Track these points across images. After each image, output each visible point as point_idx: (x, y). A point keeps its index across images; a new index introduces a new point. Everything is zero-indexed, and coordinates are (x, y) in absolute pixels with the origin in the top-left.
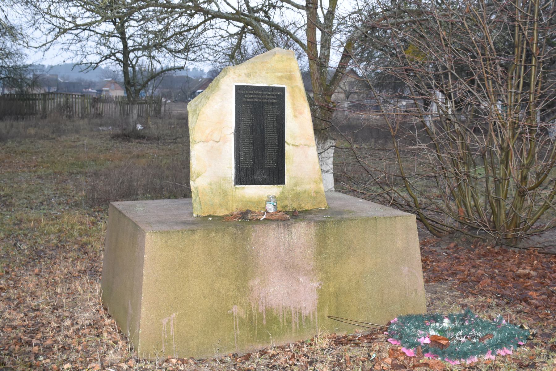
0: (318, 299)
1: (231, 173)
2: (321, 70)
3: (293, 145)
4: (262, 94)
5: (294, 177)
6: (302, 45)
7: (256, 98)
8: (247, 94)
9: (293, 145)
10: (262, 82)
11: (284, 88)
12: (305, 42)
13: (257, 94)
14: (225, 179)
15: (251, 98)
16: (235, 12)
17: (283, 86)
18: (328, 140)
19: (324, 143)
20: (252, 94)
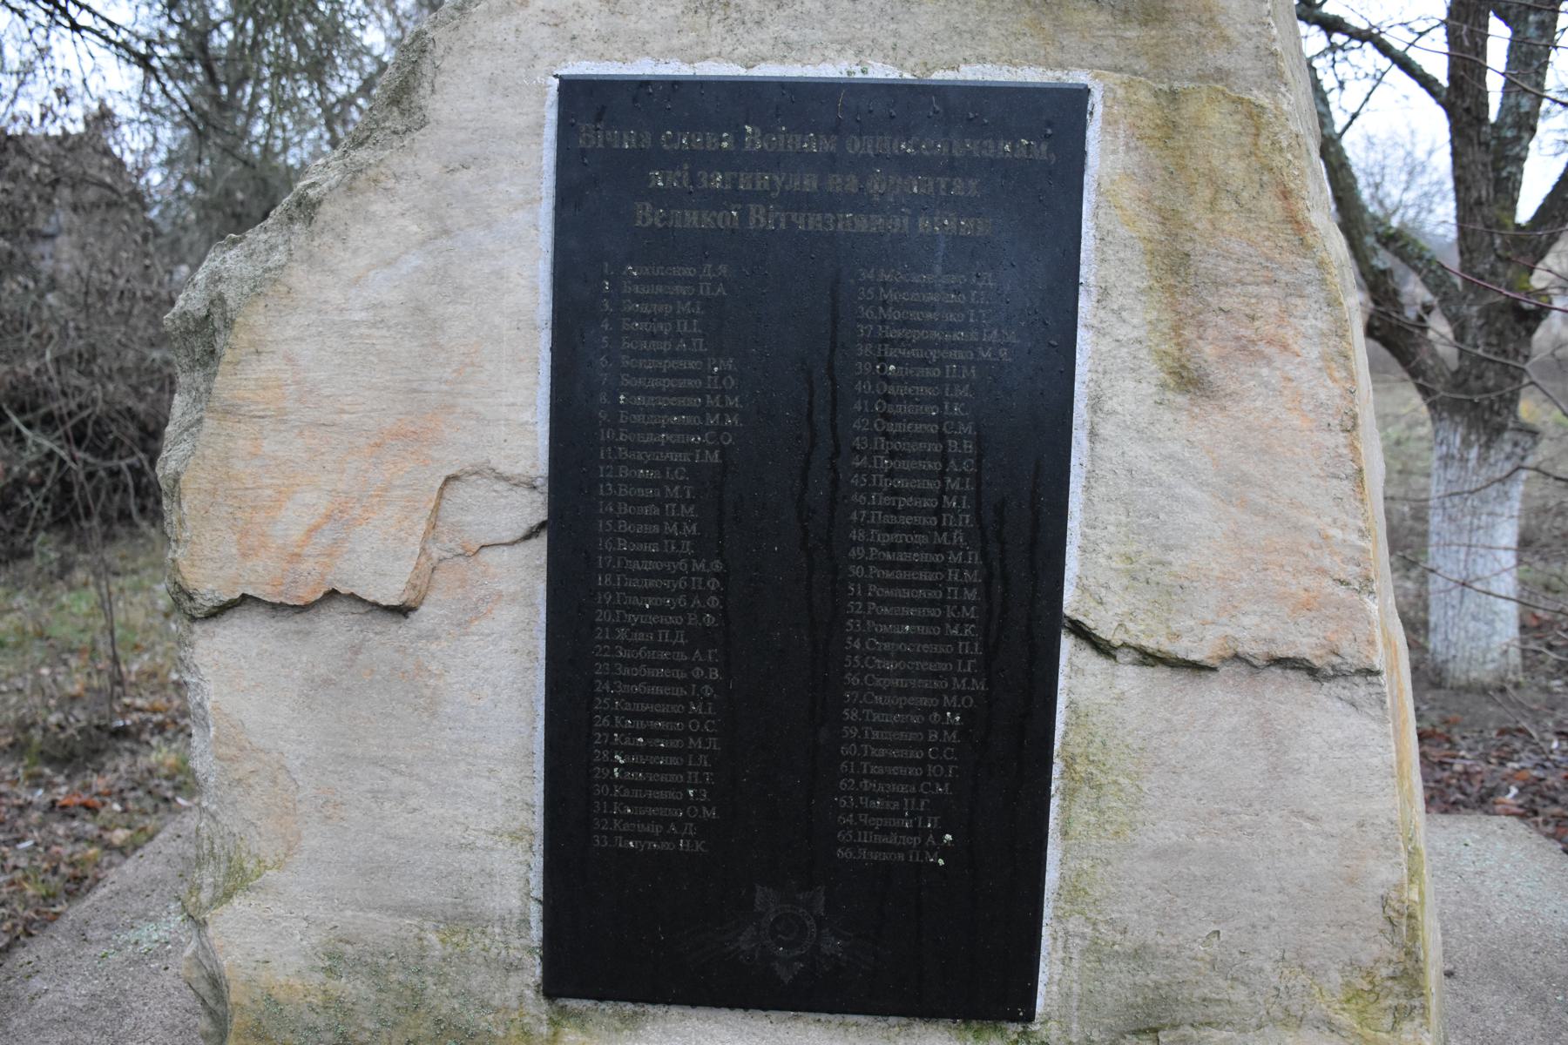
0: (1470, 427)
1: (513, 881)
2: (1497, 170)
3: (1148, 658)
4: (831, 163)
5: (1139, 954)
6: (1426, 82)
7: (762, 197)
8: (670, 161)
9: (1148, 658)
10: (844, 44)
11: (1080, 95)
12: (1438, 68)
13: (772, 161)
14: (462, 920)
15: (717, 200)
16: (1338, 129)
17: (1079, 77)
18: (1507, 435)
19: (1487, 446)
20: (722, 161)
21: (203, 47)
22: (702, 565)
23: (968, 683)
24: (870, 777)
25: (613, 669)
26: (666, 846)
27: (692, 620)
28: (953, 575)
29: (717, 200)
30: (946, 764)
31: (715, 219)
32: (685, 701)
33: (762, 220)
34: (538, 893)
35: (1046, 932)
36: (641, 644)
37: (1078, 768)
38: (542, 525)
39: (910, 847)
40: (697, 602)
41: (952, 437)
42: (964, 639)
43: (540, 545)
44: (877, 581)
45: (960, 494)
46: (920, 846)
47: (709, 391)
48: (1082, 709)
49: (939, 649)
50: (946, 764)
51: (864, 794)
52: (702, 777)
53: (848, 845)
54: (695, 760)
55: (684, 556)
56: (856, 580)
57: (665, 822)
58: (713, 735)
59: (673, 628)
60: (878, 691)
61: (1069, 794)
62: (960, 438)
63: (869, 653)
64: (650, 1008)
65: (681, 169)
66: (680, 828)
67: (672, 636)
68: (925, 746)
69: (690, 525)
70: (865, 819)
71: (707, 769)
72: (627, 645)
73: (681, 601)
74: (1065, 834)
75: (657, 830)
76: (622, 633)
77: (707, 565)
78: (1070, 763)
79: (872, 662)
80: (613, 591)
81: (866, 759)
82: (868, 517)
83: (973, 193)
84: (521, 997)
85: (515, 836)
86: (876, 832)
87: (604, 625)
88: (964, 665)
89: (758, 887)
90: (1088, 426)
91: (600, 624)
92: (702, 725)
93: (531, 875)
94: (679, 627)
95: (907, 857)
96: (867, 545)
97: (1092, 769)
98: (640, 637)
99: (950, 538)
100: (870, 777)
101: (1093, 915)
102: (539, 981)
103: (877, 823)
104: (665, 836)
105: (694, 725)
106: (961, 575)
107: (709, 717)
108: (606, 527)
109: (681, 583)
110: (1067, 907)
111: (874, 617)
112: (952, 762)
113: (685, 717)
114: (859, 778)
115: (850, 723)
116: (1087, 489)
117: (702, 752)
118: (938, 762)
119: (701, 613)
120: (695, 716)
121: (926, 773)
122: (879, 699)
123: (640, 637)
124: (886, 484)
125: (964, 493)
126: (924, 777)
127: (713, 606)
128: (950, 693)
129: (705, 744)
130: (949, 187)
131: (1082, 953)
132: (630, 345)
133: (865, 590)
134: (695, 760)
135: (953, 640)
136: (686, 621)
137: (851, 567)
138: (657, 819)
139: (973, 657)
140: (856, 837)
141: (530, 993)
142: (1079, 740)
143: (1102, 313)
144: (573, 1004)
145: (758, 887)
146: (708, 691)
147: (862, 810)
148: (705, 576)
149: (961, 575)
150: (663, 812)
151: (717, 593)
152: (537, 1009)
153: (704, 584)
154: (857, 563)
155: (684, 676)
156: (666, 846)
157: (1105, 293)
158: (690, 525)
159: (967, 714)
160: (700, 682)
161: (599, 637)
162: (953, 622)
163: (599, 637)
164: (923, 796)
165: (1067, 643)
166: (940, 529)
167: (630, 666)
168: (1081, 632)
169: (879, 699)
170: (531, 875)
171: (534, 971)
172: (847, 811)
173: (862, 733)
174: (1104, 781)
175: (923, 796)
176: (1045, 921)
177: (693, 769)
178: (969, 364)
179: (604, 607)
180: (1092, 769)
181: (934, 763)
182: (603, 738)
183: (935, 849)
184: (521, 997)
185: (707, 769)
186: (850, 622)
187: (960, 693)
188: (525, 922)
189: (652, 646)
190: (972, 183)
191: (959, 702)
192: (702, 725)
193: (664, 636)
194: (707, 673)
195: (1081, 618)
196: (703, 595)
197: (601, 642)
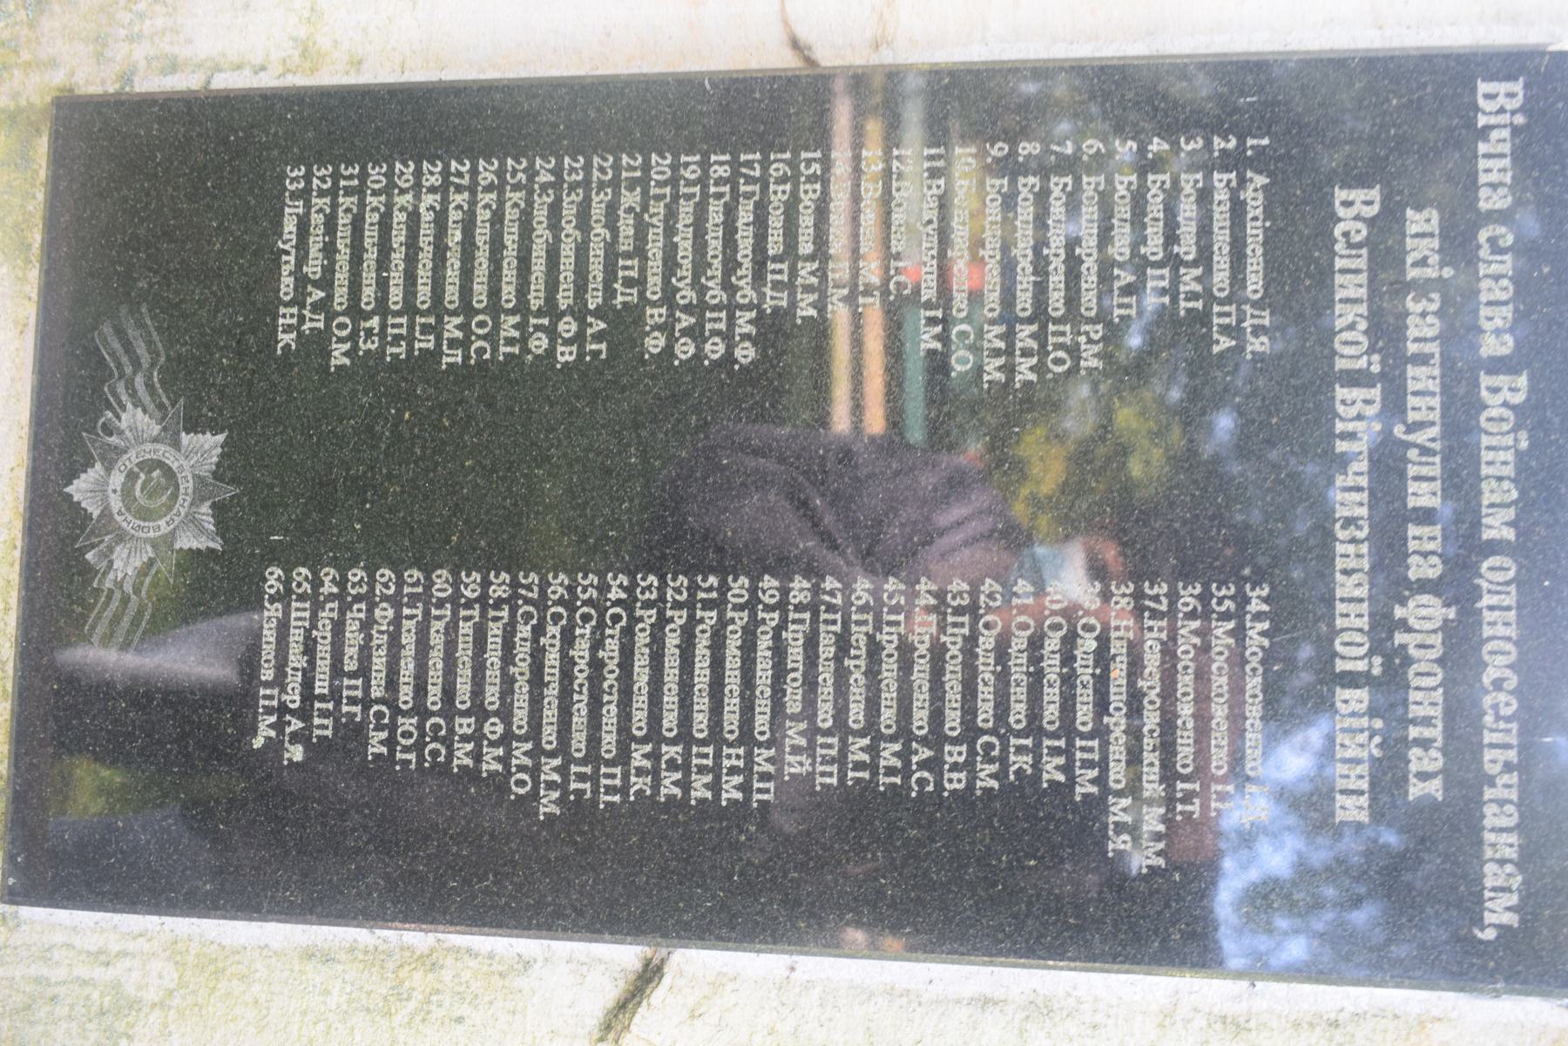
21: (1193, 394)
22: (749, 329)
23: (551, 785)
24: (397, 621)
25: (573, 187)
26: (287, 283)
27: (656, 315)
28: (733, 757)
29: (1386, 330)
30: (419, 747)
31: (1352, 327)
32: (522, 307)
33: (1353, 411)
34: (221, 82)
35: (150, 922)
36: (615, 231)
37: (418, 975)
38: (810, 62)
39: (283, 690)
40: (686, 321)
41: (972, 752)
42: (626, 776)
43: (782, 60)
44: (723, 623)
45: (873, 767)
46: (283, 709)
47: (1043, 328)
48: (520, 982)
49: (609, 740)
50: (419, 747)
51: (370, 611)
52: (397, 339)
53: (878, 599)
54: (426, 329)
55: (762, 296)
56: (724, 588)
57: (326, 282)
58: (466, 357)
59: (641, 282)
60: (539, 631)
61: (374, 959)
62: (969, 766)
63: (601, 616)
64: (34, 274)
65: (1442, 264)
66: (316, 308)
67: (628, 282)
68: (449, 710)
69: (814, 305)
70: (328, 614)
71: (410, 348)
72: (612, 208)
73: (687, 295)
74: (308, 954)
75: (313, 269)
76: (630, 199)
77: (745, 337)
78: (429, 962)
79: (586, 618)
80: (703, 181)
81: (427, 613)
82: (831, 608)
83: (1416, 790)
84: (53, 63)
85: (306, 50)
86: (308, 631)
87: (646, 167)
88: (582, 777)
89: (221, 438)
90: (998, 994)
91: (647, 162)
92: (484, 337)
93: (247, 72)
94: (642, 294)
95: (267, 685)
96: (782, 606)
97: (417, 996)
98: (627, 228)
99: (796, 750)
100: (397, 621)
101: (177, 1001)
102: (77, 92)
103: (324, 632)
104: (302, 281)
105: (481, 324)
106: (733, 771)
107: (495, 350)
108: (809, 162)
109: (716, 294)
110: (191, 959)
111: (663, 621)
112: (421, 759)
113: (495, 308)
114: (396, 602)
115: (486, 583)
116: (890, 992)
117: (439, 339)
118: (422, 734)
119: (667, 328)
120: (497, 326)
121: (405, 714)
122: (524, 631)
123: (627, 228)
124: (889, 639)
125: (875, 774)
126: (396, 711)
127: (678, 349)
128: (537, 753)
129: (453, 343)
130: (1425, 744)
131: (117, 986)
132: (1122, 190)
133: (708, 605)
134: (426, 329)
135: (623, 757)
136: (654, 304)
137: (744, 581)
138: (329, 270)
139: (595, 792)
140: (301, 598)
141: (58, 78)
142: (466, 976)
143: (1200, 1021)
144: (42, 145)
145: (221, 438)
146: (539, 343)
147: (317, 607)
148: (728, 337)
149: (733, 771)
150: (342, 277)
151: (699, 356)
152: (35, 88)
153: (715, 333)
154: (753, 590)
155: (563, 304)
156: (287, 283)
157: (1236, 1026)
158: (814, 305)
159: (499, 783)
160: (552, 332)
161: (625, 159)
162: (655, 756)
163: (625, 159)
164: (366, 709)
165: (626, 955)
166: (813, 732)
167: (578, 216)
168: (649, 975)
169: (524, 631)
170: (247, 72)
171: (95, 80)
172: (342, 583)
173: (469, 605)
174: (397, 1019)
175: (366, 709)
176: (168, 920)
177: (411, 327)
178: (1101, 781)
179: (675, 167)
180: (417, 996)
181: (420, 727)
182: (460, 175)
183: (281, 732)
184: (53, 63)
185: (410, 348)
186: (593, 578)
187: (535, 772)
188: (173, 67)
189: (611, 255)
190: (1435, 788)
191: (521, 768)
192: (484, 337)
193: (628, 268)
194: (567, 342)
195: (667, 980)
196: (697, 334)
197: (617, 167)
